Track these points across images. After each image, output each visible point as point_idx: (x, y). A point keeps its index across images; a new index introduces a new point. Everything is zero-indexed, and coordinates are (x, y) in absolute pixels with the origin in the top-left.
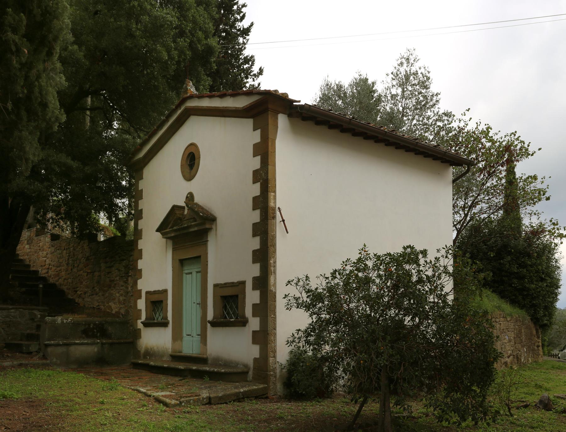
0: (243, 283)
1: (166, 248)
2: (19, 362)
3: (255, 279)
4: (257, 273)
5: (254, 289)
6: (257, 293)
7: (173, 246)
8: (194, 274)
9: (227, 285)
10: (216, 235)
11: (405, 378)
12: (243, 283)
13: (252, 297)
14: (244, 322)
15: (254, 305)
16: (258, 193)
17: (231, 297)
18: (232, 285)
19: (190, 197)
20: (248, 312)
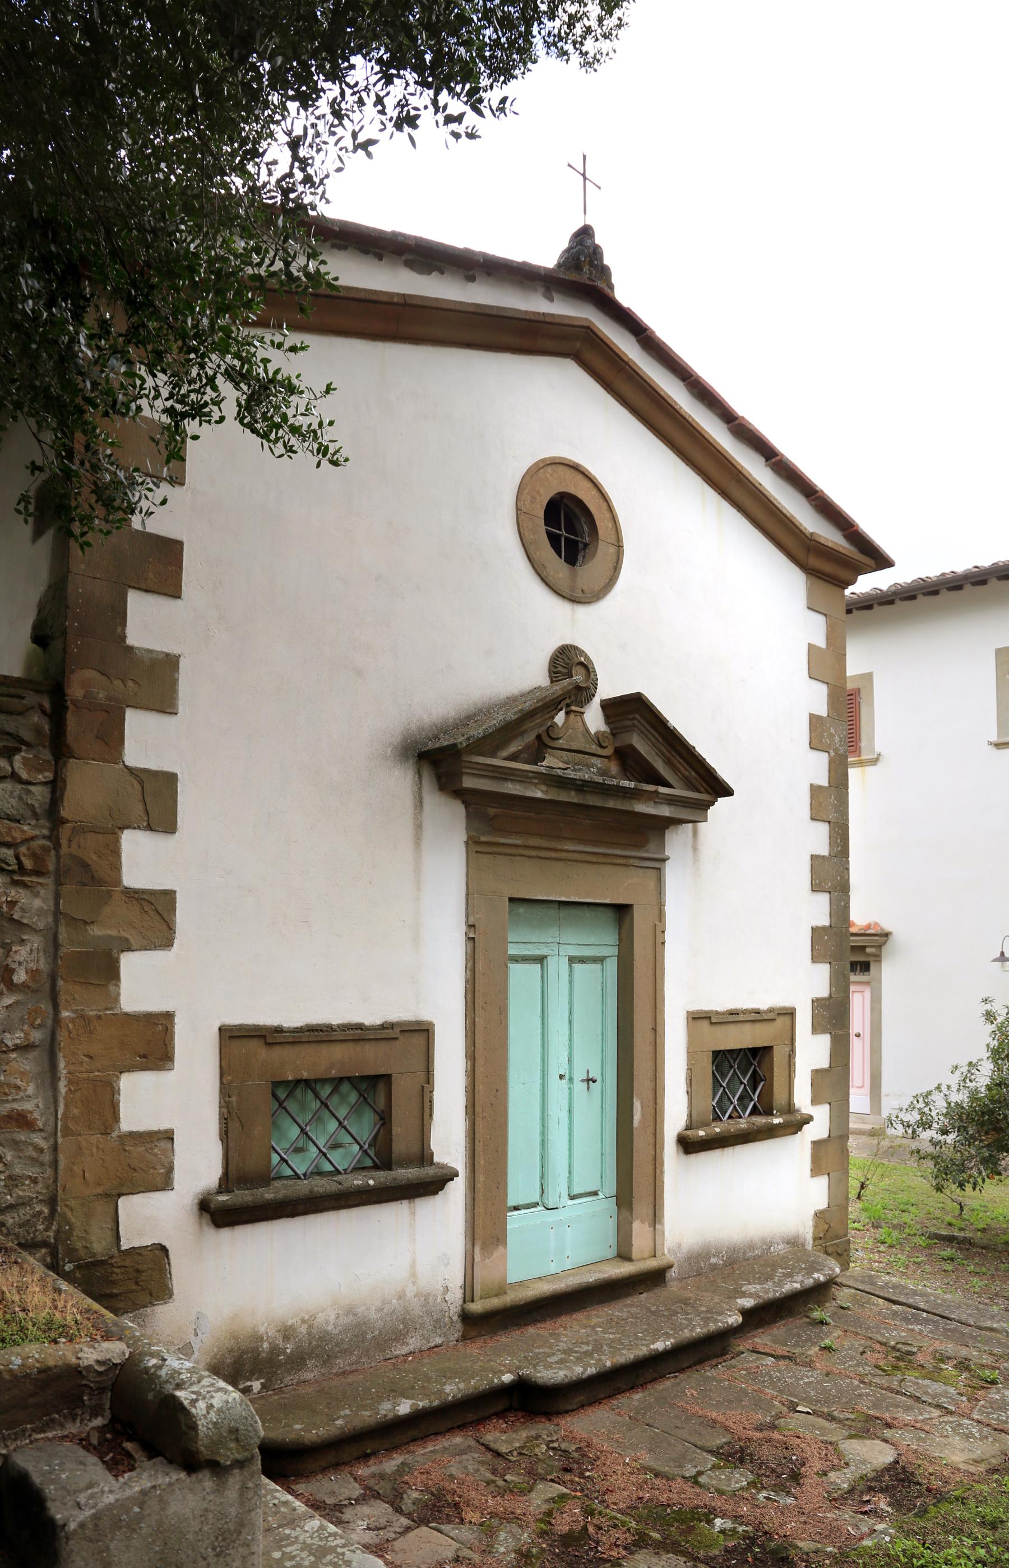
0: (790, 1013)
1: (419, 827)
2: (392, 1174)
3: (817, 1003)
4: (823, 991)
5: (816, 1029)
6: (824, 1041)
7: (468, 829)
8: (558, 966)
9: (741, 1017)
10: (695, 849)
11: (327, 448)
12: (790, 1013)
13: (811, 1051)
14: (797, 1124)
15: (816, 1073)
16: (823, 849)
17: (755, 1052)
18: (757, 1017)
19: (569, 665)
20: (802, 1097)
